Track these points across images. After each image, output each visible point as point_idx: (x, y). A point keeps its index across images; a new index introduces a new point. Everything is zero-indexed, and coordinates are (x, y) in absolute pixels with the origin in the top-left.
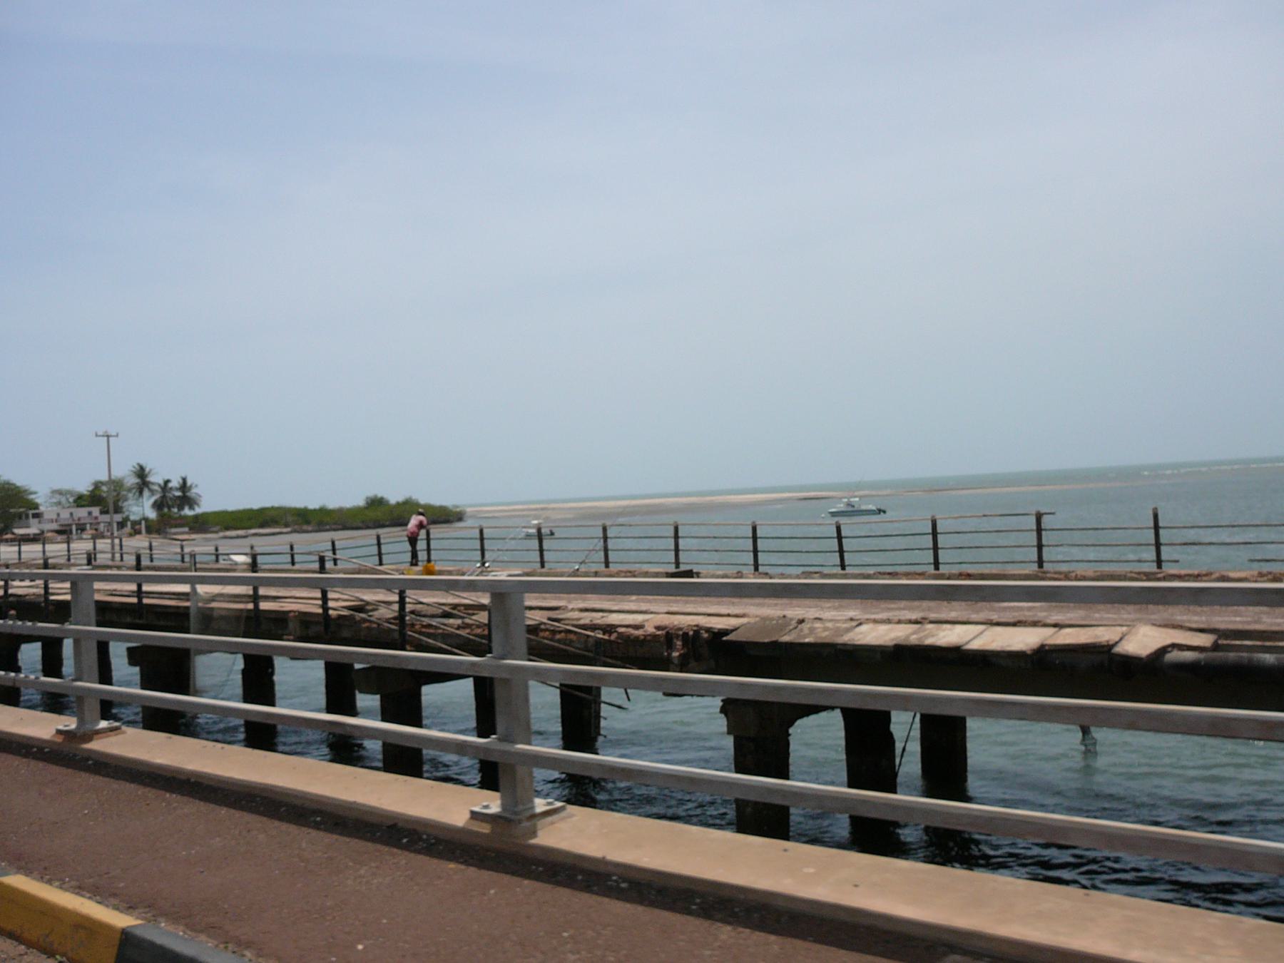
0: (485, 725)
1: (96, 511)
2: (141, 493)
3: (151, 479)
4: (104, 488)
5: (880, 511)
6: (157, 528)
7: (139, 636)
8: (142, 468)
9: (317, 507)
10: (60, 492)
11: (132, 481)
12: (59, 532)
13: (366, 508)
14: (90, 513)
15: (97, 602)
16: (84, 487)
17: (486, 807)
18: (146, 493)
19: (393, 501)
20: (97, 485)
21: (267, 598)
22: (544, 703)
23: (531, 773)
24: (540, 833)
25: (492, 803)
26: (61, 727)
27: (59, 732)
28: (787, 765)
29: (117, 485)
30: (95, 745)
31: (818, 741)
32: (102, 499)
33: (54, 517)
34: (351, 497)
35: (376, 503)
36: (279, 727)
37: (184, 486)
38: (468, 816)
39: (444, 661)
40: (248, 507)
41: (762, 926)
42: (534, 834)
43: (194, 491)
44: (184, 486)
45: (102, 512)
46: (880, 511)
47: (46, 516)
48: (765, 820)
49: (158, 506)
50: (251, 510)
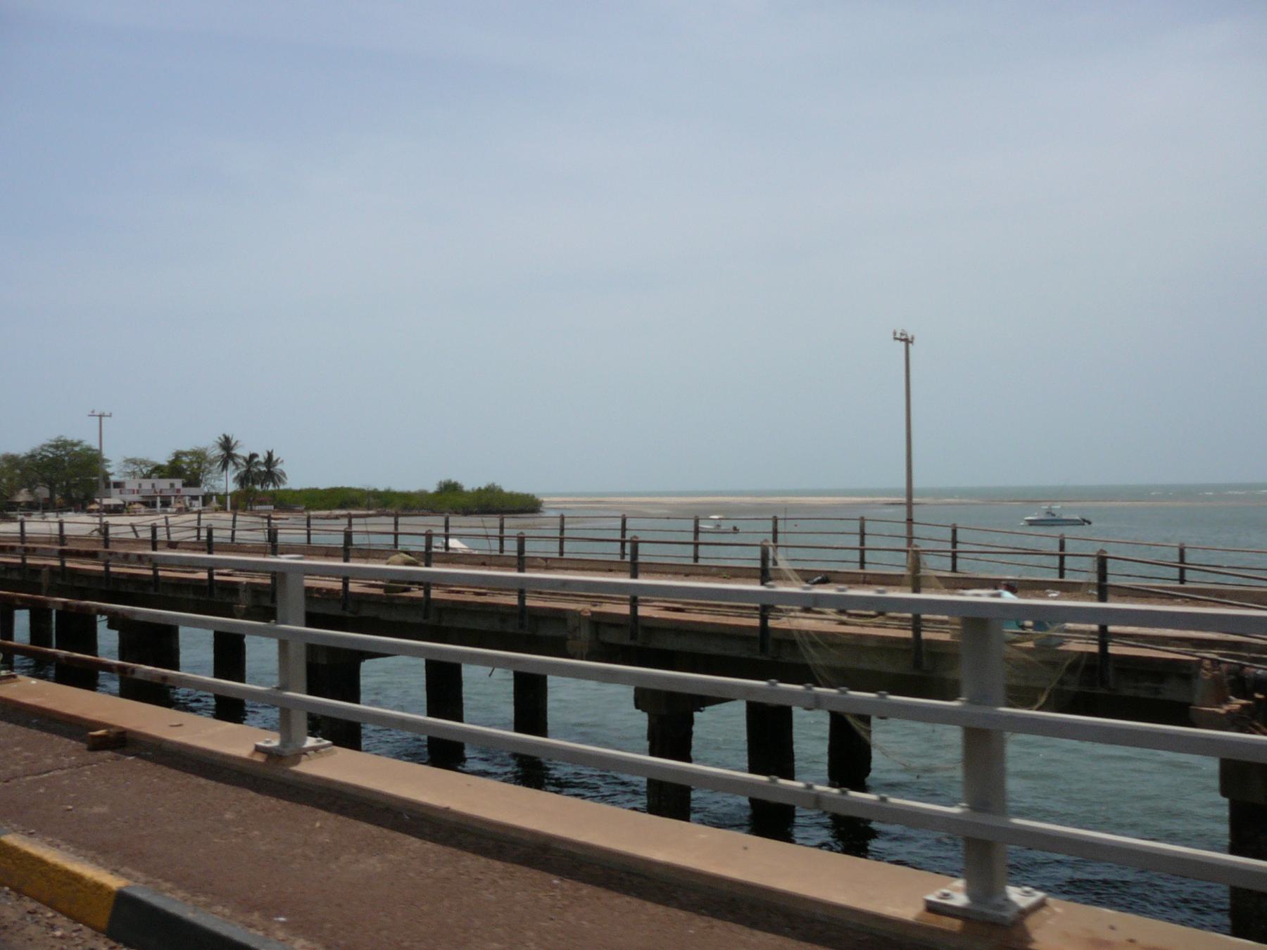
1: (178, 483)
2: (225, 466)
3: (236, 451)
4: (185, 459)
5: (1085, 522)
6: (243, 501)
7: (211, 621)
8: (227, 440)
10: (134, 462)
11: (218, 452)
12: (145, 504)
14: (172, 485)
15: (309, 590)
16: (163, 459)
17: (946, 896)
18: (231, 467)
20: (178, 455)
26: (261, 744)
27: (258, 749)
28: (689, 747)
29: (199, 456)
31: (721, 731)
32: (184, 470)
33: (136, 488)
34: (421, 479)
35: (450, 488)
36: (247, 702)
37: (270, 460)
38: (921, 907)
39: (370, 641)
40: (313, 486)
41: (342, 811)
43: (279, 467)
44: (270, 460)
45: (184, 485)
46: (1085, 522)
47: (128, 486)
48: (670, 800)
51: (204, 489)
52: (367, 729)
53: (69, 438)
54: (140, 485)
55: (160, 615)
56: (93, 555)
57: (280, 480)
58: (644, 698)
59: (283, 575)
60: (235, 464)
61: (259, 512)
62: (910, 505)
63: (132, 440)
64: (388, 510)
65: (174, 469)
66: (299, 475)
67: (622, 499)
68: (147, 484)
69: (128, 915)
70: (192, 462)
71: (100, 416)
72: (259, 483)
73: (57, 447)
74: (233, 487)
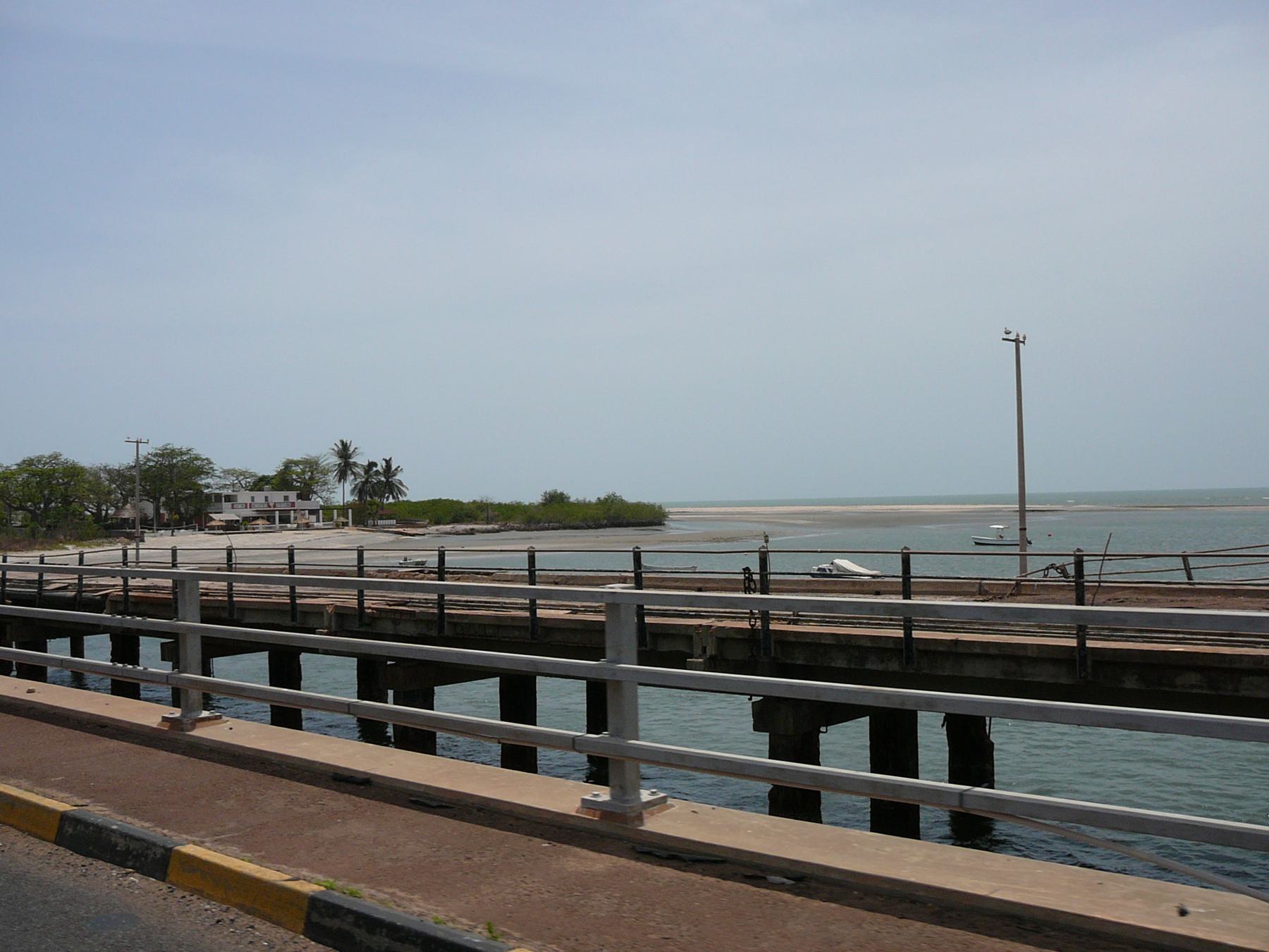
0: (596, 721)
1: (292, 496)
8: (345, 446)
9: (634, 501)
11: (336, 460)
13: (543, 504)
14: (286, 498)
16: (270, 468)
17: (595, 796)
19: (572, 499)
20: (288, 465)
21: (651, 613)
22: (932, 740)
23: (638, 767)
24: (645, 821)
25: (603, 794)
27: (165, 719)
30: (200, 732)
32: (296, 480)
34: (531, 496)
35: (555, 500)
38: (578, 804)
42: (642, 824)
45: (299, 497)
49: (361, 491)
50: (458, 502)
51: (317, 501)
52: (827, 798)
53: (177, 446)
54: (253, 498)
55: (888, 696)
56: (113, 574)
57: (401, 492)
58: (767, 714)
59: (183, 582)
60: (353, 473)
61: (383, 526)
62: (1023, 512)
63: (238, 448)
64: (511, 524)
65: (282, 481)
66: (418, 486)
67: (729, 509)
68: (259, 497)
69: (319, 916)
70: (304, 472)
71: (1017, 341)
72: (377, 497)
73: (162, 455)
74: (350, 498)
